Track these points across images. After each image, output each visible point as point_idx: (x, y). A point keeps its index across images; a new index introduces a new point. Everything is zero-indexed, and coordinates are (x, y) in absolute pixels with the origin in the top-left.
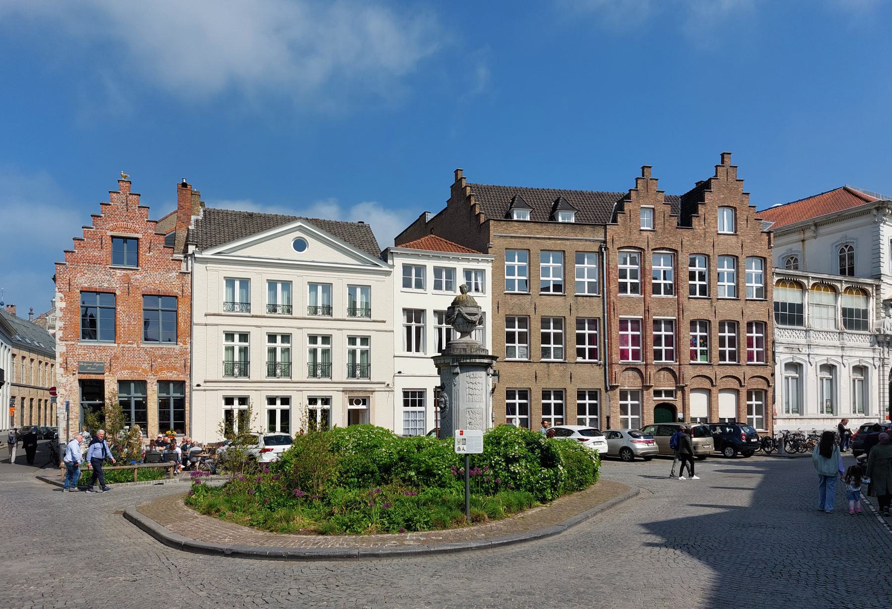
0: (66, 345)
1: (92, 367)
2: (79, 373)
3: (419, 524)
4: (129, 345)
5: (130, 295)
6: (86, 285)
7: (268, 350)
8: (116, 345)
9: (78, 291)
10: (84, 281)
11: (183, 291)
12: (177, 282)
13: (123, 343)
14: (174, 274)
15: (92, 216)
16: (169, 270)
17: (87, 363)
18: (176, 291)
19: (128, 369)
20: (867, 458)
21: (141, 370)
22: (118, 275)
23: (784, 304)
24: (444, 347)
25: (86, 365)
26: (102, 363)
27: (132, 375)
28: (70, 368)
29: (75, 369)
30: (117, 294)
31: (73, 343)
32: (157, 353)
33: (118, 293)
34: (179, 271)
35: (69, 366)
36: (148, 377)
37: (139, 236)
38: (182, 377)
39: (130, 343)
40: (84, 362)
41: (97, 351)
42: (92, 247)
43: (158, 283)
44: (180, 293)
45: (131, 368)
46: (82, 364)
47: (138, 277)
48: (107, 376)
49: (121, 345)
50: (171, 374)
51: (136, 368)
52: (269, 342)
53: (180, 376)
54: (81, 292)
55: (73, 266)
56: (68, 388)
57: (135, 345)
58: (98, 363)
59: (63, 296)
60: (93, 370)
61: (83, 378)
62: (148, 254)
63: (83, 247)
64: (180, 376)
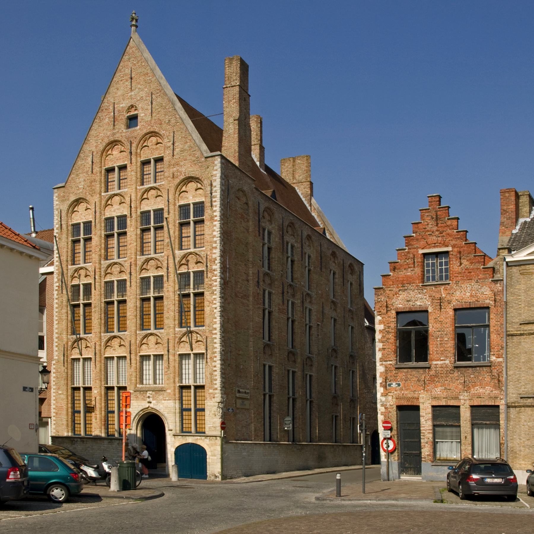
30: (430, 311)
37: (449, 249)
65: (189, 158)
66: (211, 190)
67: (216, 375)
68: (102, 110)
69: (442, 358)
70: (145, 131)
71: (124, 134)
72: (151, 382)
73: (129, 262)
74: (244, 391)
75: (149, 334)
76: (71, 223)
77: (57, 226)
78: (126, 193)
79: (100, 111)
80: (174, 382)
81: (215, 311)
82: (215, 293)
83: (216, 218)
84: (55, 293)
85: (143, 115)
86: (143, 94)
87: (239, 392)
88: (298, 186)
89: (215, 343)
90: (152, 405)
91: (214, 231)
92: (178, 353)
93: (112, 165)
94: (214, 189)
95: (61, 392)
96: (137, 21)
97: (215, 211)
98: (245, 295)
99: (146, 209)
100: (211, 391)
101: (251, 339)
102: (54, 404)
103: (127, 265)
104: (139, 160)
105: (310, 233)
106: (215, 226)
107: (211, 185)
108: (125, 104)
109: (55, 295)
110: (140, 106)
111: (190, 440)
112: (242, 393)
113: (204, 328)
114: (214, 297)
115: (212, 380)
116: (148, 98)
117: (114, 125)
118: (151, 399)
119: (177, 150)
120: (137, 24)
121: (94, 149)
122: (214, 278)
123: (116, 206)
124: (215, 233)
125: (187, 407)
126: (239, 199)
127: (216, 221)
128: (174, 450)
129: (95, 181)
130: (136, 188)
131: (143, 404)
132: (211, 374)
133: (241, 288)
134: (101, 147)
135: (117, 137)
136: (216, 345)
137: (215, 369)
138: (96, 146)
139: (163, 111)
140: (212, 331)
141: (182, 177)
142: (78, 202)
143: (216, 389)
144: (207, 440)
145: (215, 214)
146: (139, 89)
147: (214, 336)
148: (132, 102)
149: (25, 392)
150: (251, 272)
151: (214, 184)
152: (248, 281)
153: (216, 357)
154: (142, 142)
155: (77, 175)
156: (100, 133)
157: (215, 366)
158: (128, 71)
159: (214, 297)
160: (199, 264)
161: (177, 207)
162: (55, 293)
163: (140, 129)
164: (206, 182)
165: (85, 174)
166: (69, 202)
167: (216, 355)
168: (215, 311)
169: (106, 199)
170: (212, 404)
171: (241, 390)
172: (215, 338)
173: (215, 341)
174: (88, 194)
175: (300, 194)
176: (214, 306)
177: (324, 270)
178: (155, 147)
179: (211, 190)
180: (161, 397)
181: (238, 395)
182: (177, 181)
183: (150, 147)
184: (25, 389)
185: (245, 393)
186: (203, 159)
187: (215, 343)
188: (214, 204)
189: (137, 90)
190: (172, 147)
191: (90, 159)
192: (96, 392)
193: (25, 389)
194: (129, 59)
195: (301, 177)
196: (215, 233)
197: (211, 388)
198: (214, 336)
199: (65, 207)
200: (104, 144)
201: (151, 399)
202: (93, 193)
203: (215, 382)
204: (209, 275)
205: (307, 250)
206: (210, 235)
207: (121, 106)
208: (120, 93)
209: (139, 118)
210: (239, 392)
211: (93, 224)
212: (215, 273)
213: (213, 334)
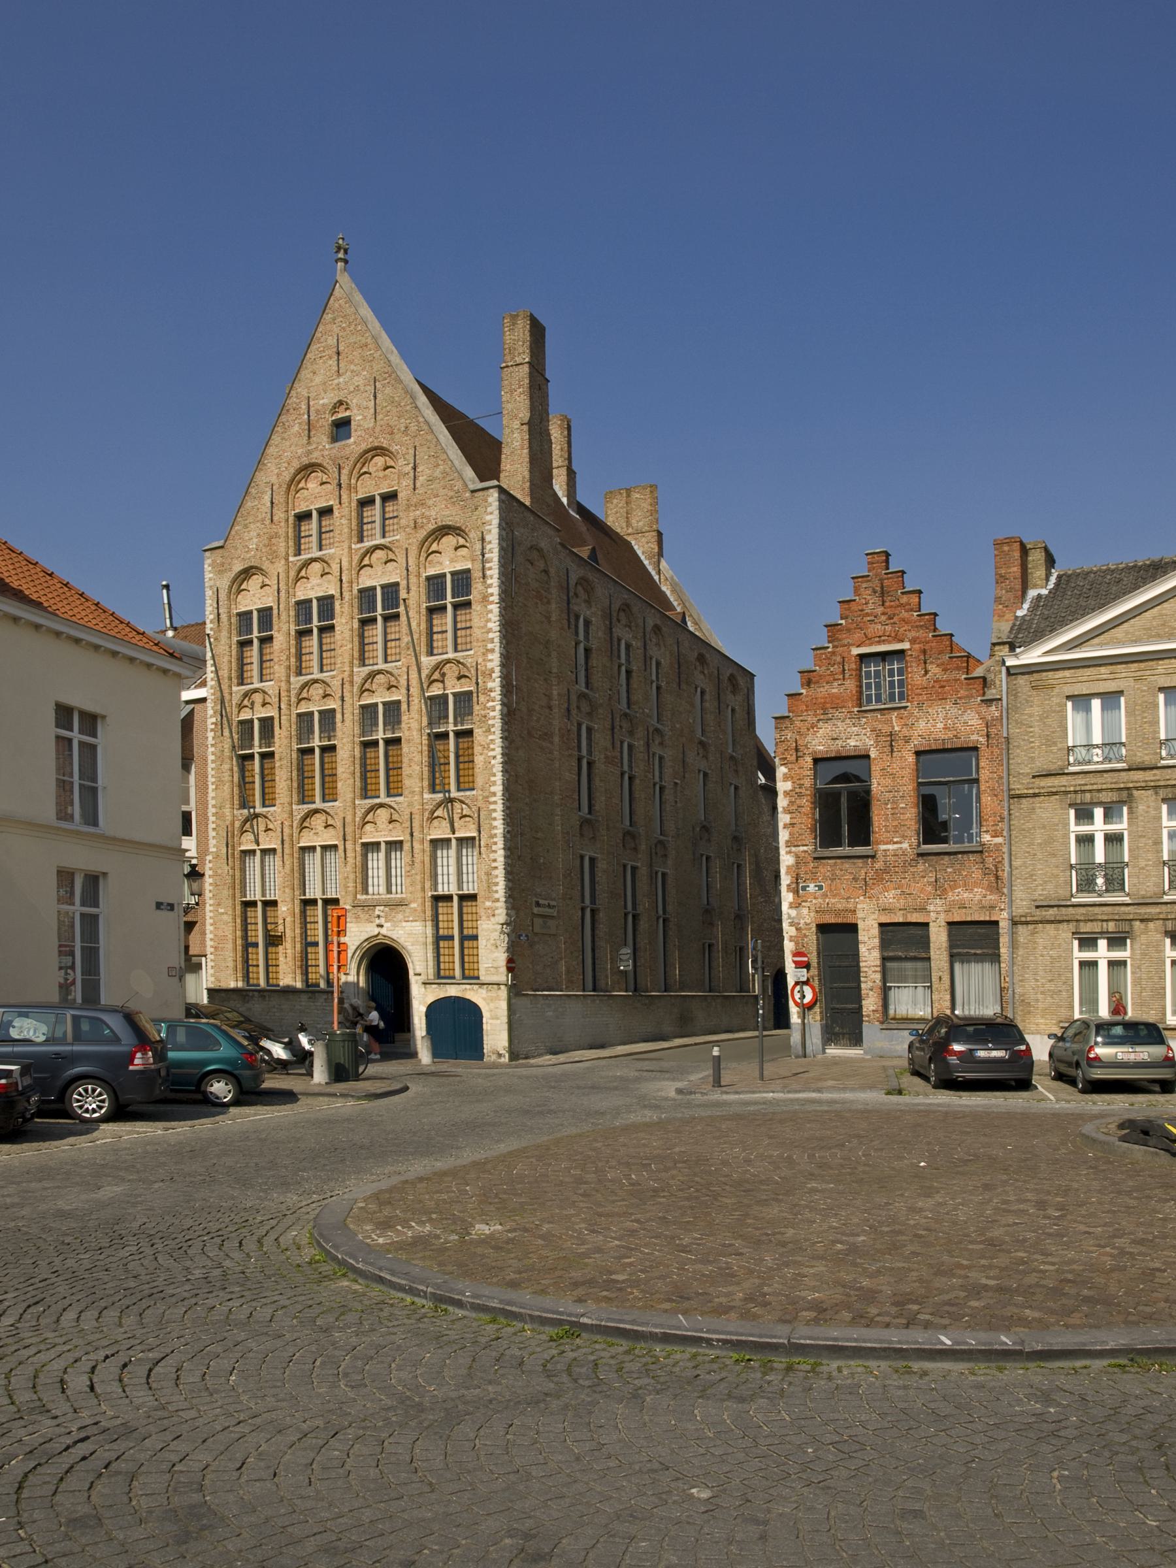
3: (806, 1001)
5: (895, 754)
6: (822, 748)
10: (820, 742)
11: (988, 736)
15: (826, 626)
18: (974, 737)
23: (829, 636)
30: (873, 756)
33: (873, 754)
39: (896, 843)
52: (57, 726)
53: (989, 897)
64: (989, 897)
65: (442, 492)
66: (483, 548)
67: (497, 876)
68: (288, 411)
69: (895, 840)
70: (364, 447)
71: (326, 453)
72: (383, 889)
73: (339, 678)
74: (546, 902)
75: (377, 804)
76: (235, 612)
77: (212, 617)
78: (332, 556)
79: (284, 412)
80: (423, 889)
81: (493, 762)
82: (492, 730)
83: (491, 599)
84: (210, 735)
85: (359, 418)
86: (359, 381)
87: (538, 904)
88: (636, 539)
89: (495, 819)
90: (384, 931)
91: (489, 620)
92: (429, 838)
93: (307, 506)
94: (488, 547)
95: (222, 911)
96: (346, 252)
97: (490, 586)
98: (546, 734)
99: (369, 583)
100: (488, 904)
101: (558, 811)
102: (211, 932)
103: (336, 684)
104: (355, 497)
105: (659, 622)
106: (491, 611)
107: (483, 539)
108: (327, 400)
109: (210, 739)
110: (354, 402)
111: (453, 991)
112: (544, 906)
113: (474, 792)
114: (491, 737)
115: (490, 885)
116: (368, 388)
117: (309, 437)
118: (382, 921)
119: (421, 479)
120: (347, 257)
121: (274, 479)
122: (491, 704)
123: (315, 580)
124: (490, 625)
125: (446, 933)
126: (532, 564)
127: (492, 603)
128: (424, 1009)
129: (277, 535)
130: (350, 548)
131: (369, 929)
132: (488, 874)
133: (538, 720)
134: (287, 476)
135: (316, 457)
136: (495, 823)
137: (494, 865)
138: (278, 475)
139: (395, 410)
140: (487, 797)
141: (431, 527)
142: (247, 573)
143: (497, 900)
144: (483, 992)
145: (490, 591)
146: (352, 371)
147: (492, 807)
148: (341, 396)
149: (159, 912)
150: (555, 693)
151: (488, 538)
152: (550, 708)
153: (495, 843)
154: (359, 465)
155: (246, 526)
156: (284, 451)
157: (495, 860)
158: (332, 341)
159: (491, 737)
160: (463, 680)
161: (423, 579)
162: (210, 735)
163: (355, 443)
164: (474, 535)
165: (258, 524)
166: (232, 575)
167: (495, 840)
168: (493, 762)
169: (296, 568)
170: (491, 927)
171: (541, 902)
172: (495, 810)
173: (494, 815)
174: (264, 559)
175: (639, 553)
176: (491, 754)
177: (684, 686)
178: (381, 474)
179: (483, 548)
180: (400, 916)
181: (536, 910)
182: (422, 534)
183: (373, 475)
184: (159, 905)
185: (549, 906)
186: (468, 495)
187: (495, 819)
188: (488, 573)
189: (349, 373)
190: (412, 474)
191: (267, 498)
192: (284, 909)
193: (159, 905)
194: (334, 319)
195: (641, 524)
196: (490, 625)
197: (488, 899)
198: (492, 807)
199: (224, 583)
200: (292, 471)
201: (382, 921)
202: (273, 557)
203: (495, 888)
204: (482, 699)
205: (654, 652)
206: (482, 628)
207: (321, 402)
208: (318, 379)
209: (353, 423)
210: (538, 904)
211: (275, 612)
212: (493, 694)
213: (490, 803)
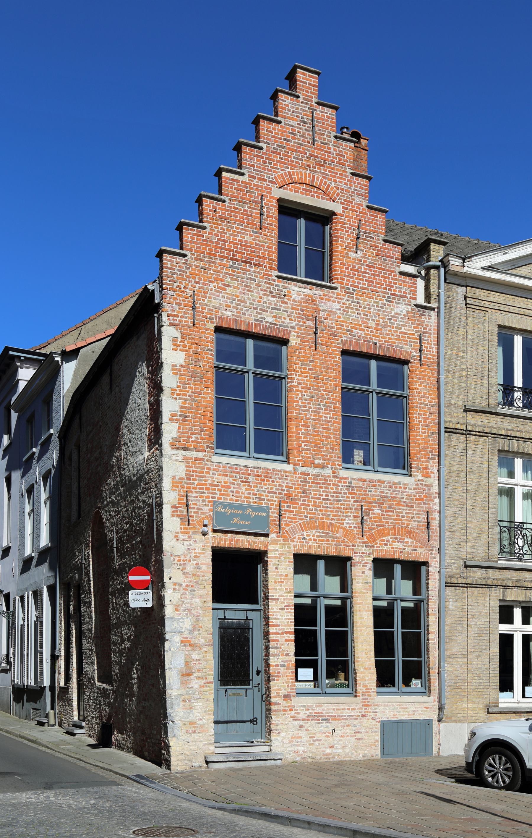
0: (186, 460)
1: (243, 517)
2: (215, 531)
4: (317, 470)
6: (229, 314)
7: (508, 478)
8: (289, 468)
9: (212, 327)
12: (409, 328)
13: (306, 465)
14: (402, 308)
16: (392, 299)
17: (231, 506)
18: (407, 348)
19: (315, 528)
20: (44, 360)
21: (341, 531)
22: (294, 296)
24: (11, 353)
25: (229, 511)
26: (263, 510)
27: (324, 544)
28: (195, 519)
29: (206, 522)
31: (201, 455)
32: (374, 493)
34: (413, 302)
35: (192, 512)
36: (356, 549)
37: (336, 207)
38: (419, 555)
39: (318, 466)
40: (225, 506)
41: (251, 479)
42: (241, 222)
43: (373, 325)
44: (416, 354)
45: (322, 526)
46: (220, 509)
47: (335, 306)
48: (275, 543)
49: (301, 469)
50: (401, 545)
51: (331, 527)
53: (420, 550)
54: (218, 330)
55: (201, 264)
56: (190, 568)
57: (328, 472)
58: (254, 509)
59: (178, 335)
60: (245, 525)
61: (223, 544)
62: (353, 255)
63: (223, 218)
64: (420, 550)
